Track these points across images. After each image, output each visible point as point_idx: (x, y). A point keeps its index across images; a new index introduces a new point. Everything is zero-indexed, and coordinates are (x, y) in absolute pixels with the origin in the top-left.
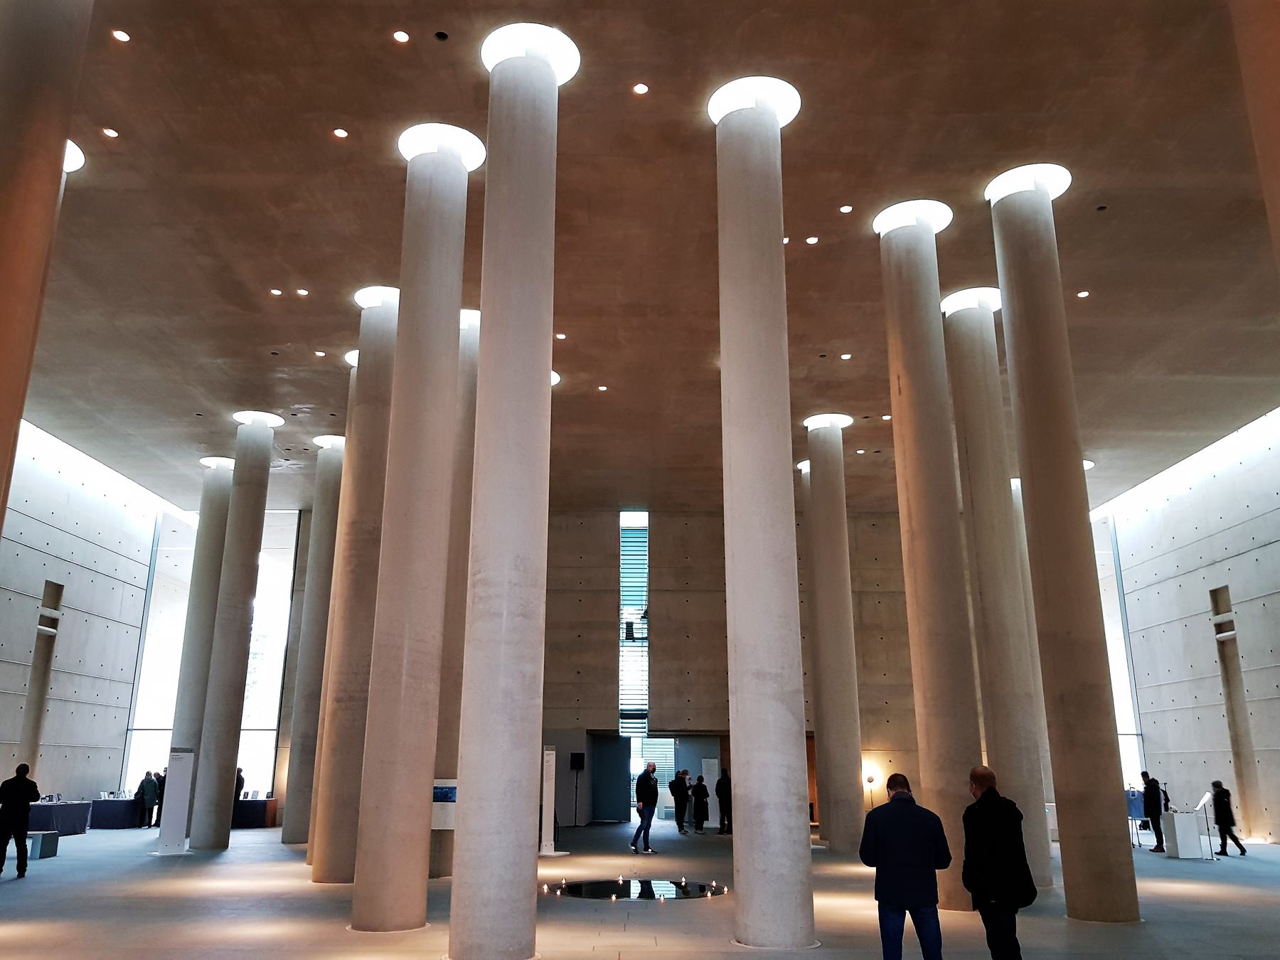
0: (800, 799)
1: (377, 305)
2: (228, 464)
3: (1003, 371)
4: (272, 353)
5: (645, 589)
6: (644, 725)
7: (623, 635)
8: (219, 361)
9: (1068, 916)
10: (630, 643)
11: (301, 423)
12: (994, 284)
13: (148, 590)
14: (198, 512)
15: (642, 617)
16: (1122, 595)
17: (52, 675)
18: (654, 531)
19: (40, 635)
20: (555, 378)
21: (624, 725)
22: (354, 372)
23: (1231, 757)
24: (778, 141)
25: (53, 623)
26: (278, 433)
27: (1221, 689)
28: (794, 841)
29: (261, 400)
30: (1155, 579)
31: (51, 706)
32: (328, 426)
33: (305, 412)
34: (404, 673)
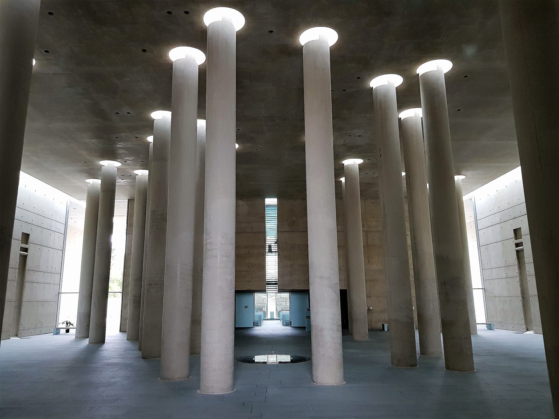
0: (338, 326)
1: (160, 118)
2: (99, 182)
3: (424, 141)
4: (116, 137)
5: (276, 231)
6: (276, 289)
7: (267, 250)
8: (93, 141)
9: (446, 369)
10: (270, 254)
11: (128, 165)
12: (419, 106)
13: (65, 234)
14: (86, 201)
15: (276, 243)
16: (477, 230)
17: (27, 272)
18: (280, 207)
19: (21, 255)
20: (237, 146)
21: (268, 288)
22: (151, 145)
23: (520, 298)
24: (329, 53)
25: (26, 250)
26: (118, 169)
27: (517, 271)
28: (336, 343)
29: (112, 156)
30: (491, 224)
31: (27, 285)
32: (140, 166)
33: (130, 160)
34: (178, 277)
